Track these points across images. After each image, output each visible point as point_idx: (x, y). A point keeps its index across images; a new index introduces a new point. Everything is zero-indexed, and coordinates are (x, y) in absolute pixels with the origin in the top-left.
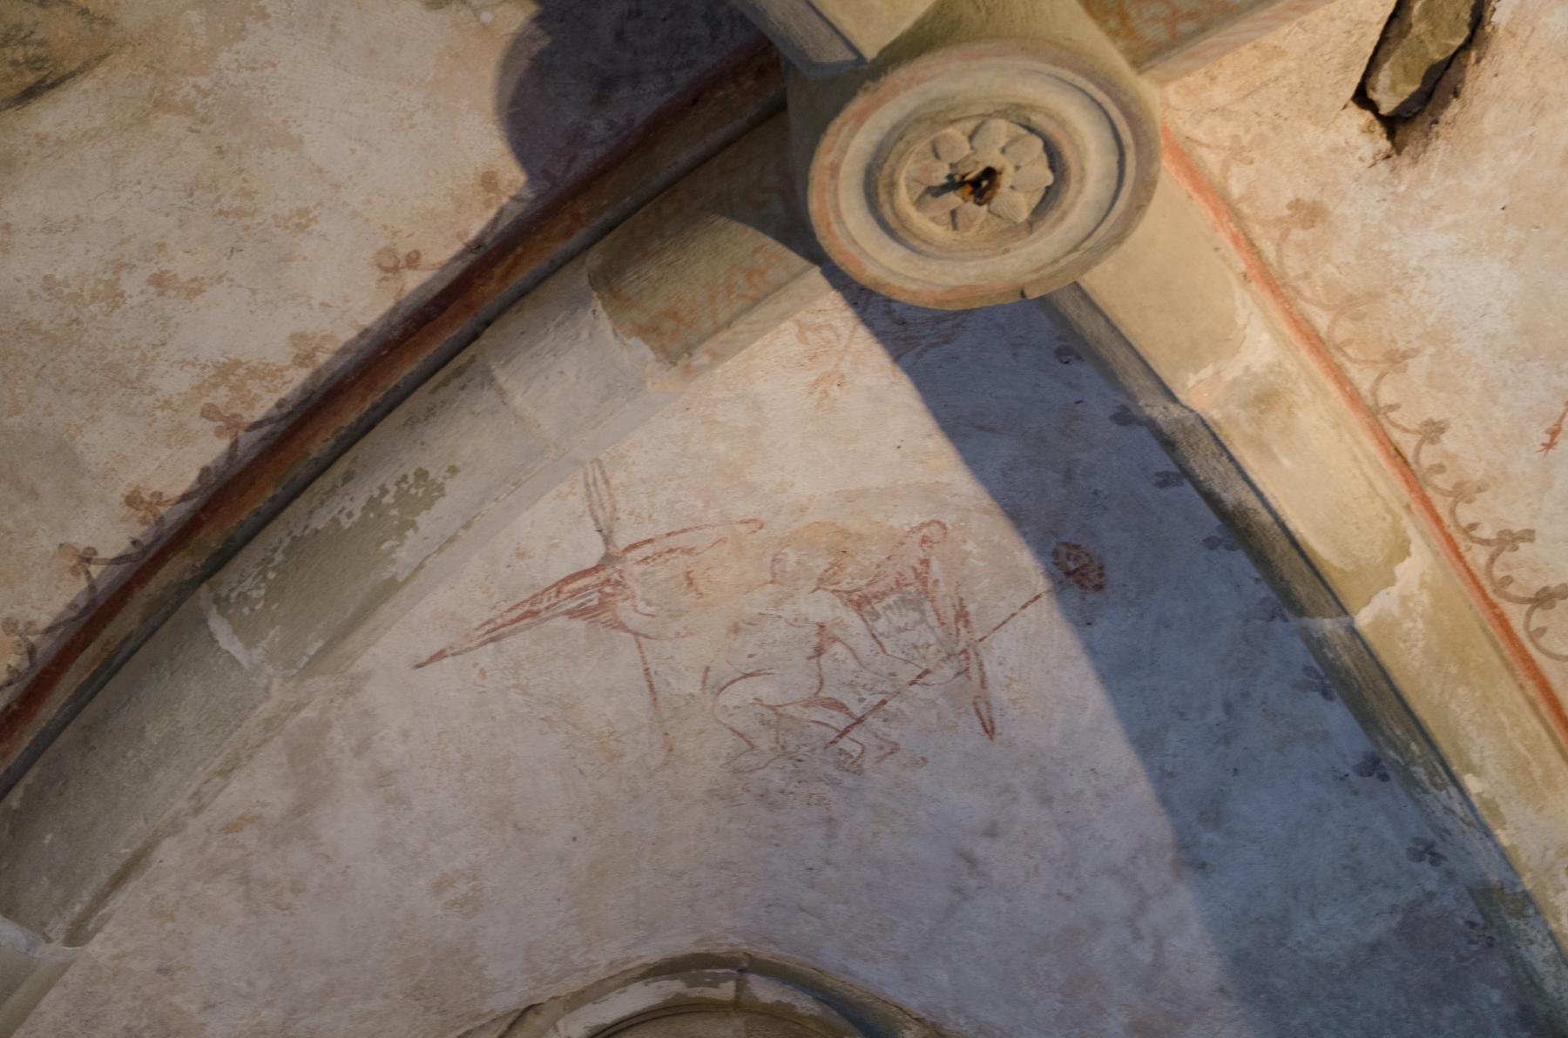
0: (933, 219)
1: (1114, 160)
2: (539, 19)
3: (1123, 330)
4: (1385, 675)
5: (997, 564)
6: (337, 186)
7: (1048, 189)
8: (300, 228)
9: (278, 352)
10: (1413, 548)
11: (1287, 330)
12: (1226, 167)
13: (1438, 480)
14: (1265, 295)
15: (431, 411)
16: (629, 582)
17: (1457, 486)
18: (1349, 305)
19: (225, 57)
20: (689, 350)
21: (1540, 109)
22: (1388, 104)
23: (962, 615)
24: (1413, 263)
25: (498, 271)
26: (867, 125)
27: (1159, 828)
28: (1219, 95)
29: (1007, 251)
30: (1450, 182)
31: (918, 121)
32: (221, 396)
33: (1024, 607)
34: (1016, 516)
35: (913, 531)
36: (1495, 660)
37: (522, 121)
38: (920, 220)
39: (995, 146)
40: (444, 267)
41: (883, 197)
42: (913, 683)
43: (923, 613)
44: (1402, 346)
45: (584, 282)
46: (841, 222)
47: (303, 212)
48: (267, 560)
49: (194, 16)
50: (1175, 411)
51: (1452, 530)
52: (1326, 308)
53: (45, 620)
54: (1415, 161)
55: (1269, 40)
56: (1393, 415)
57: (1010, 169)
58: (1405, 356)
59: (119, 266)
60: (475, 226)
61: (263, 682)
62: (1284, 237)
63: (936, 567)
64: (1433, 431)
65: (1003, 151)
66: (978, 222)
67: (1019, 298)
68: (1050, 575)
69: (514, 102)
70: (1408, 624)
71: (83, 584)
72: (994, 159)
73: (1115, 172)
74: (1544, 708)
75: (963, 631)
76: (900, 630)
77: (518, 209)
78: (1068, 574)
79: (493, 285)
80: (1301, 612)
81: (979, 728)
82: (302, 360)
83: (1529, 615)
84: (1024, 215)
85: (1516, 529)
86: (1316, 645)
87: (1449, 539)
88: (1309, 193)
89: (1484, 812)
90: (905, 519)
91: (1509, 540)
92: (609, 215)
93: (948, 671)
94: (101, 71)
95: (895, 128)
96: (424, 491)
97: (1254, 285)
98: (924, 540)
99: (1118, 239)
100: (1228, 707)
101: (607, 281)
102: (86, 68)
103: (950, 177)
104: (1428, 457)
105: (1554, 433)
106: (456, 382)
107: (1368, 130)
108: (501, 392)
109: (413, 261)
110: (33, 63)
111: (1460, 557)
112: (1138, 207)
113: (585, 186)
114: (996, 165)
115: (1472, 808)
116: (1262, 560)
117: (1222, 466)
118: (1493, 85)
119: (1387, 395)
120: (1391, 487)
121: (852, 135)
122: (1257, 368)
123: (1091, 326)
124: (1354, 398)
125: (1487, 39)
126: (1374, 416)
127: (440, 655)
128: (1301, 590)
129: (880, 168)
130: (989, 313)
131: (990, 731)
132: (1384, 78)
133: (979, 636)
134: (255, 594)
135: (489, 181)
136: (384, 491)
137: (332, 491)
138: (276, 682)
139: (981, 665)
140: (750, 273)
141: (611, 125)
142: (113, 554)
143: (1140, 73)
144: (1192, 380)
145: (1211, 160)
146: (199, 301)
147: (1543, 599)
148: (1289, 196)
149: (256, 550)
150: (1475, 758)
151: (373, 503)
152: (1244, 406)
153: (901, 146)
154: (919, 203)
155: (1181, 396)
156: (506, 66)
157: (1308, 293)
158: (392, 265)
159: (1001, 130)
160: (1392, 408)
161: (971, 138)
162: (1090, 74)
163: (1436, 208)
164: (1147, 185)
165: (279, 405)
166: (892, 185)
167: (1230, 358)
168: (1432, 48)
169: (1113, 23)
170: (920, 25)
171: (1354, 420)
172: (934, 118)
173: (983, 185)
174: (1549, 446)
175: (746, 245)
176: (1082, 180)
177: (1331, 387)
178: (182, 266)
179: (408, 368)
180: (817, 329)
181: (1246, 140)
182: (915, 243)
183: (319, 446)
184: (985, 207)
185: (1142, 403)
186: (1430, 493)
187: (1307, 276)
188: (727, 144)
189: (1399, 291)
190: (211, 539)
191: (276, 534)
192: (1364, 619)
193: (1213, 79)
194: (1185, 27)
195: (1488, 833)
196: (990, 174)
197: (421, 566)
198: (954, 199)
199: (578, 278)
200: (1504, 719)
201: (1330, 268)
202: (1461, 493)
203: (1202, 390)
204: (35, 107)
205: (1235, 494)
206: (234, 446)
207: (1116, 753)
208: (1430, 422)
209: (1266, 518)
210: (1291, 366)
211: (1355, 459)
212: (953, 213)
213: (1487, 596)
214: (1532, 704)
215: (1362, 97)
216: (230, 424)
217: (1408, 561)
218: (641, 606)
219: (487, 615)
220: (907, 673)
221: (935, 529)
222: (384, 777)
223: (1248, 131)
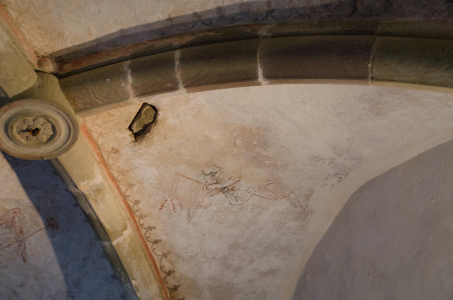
0: (22, 138)
1: (68, 132)
3: (67, 170)
4: (117, 256)
5: (32, 219)
7: (52, 136)
10: (128, 228)
11: (107, 175)
12: (98, 137)
13: (137, 213)
14: (103, 167)
17: (141, 215)
18: (122, 172)
21: (165, 138)
22: (135, 131)
23: (22, 232)
24: (137, 165)
26: (7, 113)
27: (64, 287)
28: (99, 122)
29: (39, 148)
30: (146, 150)
33: (38, 231)
34: (39, 209)
35: (12, 210)
36: (143, 255)
38: (18, 137)
41: (9, 130)
42: (6, 247)
43: (11, 230)
44: (132, 183)
50: (77, 191)
51: (138, 224)
52: (117, 172)
54: (139, 144)
55: (111, 112)
56: (129, 198)
57: (43, 129)
58: (133, 185)
62: (110, 155)
63: (16, 219)
64: (137, 202)
65: (41, 125)
66: (33, 140)
67: (41, 159)
68: (45, 224)
70: (124, 245)
72: (39, 126)
73: (68, 134)
74: (152, 266)
75: (21, 235)
76: (5, 234)
78: (50, 224)
80: (101, 240)
81: (22, 259)
83: (153, 245)
84: (45, 140)
85: (152, 226)
86: (104, 247)
87: (138, 227)
88: (116, 146)
89: (135, 289)
90: (10, 206)
91: (150, 228)
93: (16, 245)
95: (14, 115)
97: (101, 165)
98: (14, 212)
99: (67, 149)
100: (84, 260)
103: (27, 128)
104: (135, 208)
105: (162, 206)
107: (130, 135)
111: (139, 231)
112: (73, 143)
115: (133, 288)
116: (94, 227)
117: (87, 205)
118: (157, 132)
119: (128, 193)
120: (125, 213)
121: (3, 114)
122: (98, 183)
123: (59, 168)
124: (121, 193)
125: (156, 122)
126: (125, 198)
128: (102, 235)
129: (9, 123)
131: (25, 260)
132: (135, 125)
133: (25, 237)
139: (25, 244)
143: (77, 114)
144: (82, 184)
145: (95, 136)
147: (156, 242)
148: (111, 146)
150: (135, 277)
152: (94, 191)
153: (15, 119)
155: (79, 187)
157: (113, 168)
159: (41, 120)
160: (129, 196)
161: (34, 120)
162: (65, 112)
163: (143, 155)
164: (75, 139)
166: (12, 128)
167: (91, 180)
168: (145, 121)
169: (72, 102)
170: (24, 92)
171: (120, 198)
172: (25, 114)
173: (35, 132)
174: (161, 209)
176: (60, 135)
177: (116, 190)
181: (103, 132)
182: (17, 142)
184: (35, 137)
185: (70, 187)
186: (135, 216)
187: (113, 164)
189: (133, 171)
192: (114, 243)
193: (98, 118)
194: (88, 106)
195: (135, 294)
198: (28, 134)
200: (142, 268)
201: (119, 164)
202: (141, 217)
203: (84, 187)
205: (89, 211)
207: (56, 269)
208: (136, 201)
209: (95, 217)
210: (106, 184)
211: (118, 207)
212: (27, 137)
213: (144, 240)
214: (150, 265)
215: (130, 128)
217: (126, 231)
220: (5, 244)
221: (17, 210)
223: (104, 130)
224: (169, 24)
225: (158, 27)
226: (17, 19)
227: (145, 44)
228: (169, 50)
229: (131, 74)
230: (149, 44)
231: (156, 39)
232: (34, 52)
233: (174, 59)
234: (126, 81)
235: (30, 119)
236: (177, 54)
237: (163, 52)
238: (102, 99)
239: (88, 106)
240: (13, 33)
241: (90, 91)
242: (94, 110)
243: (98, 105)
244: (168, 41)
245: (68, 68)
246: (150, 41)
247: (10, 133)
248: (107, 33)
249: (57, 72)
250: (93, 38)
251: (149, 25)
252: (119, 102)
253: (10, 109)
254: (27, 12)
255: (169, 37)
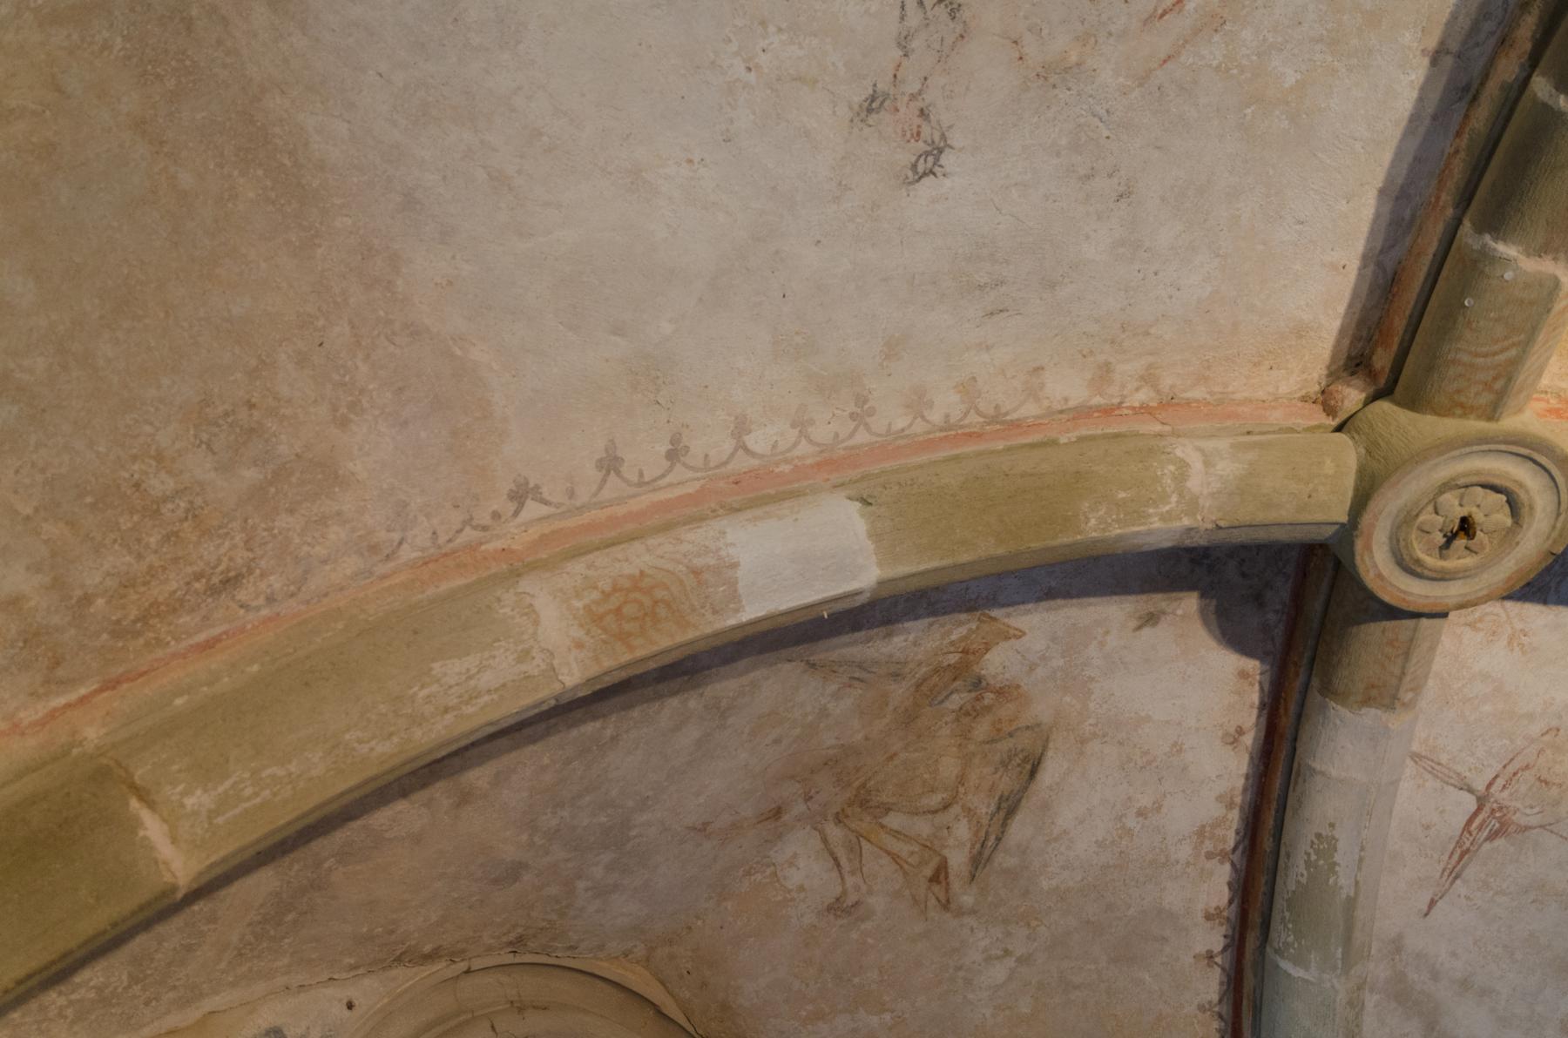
2: (1202, 596)
6: (1179, 724)
7: (1508, 502)
8: (1180, 751)
9: (1217, 811)
15: (1300, 801)
16: (1507, 803)
19: (1092, 705)
20: (1395, 697)
25: (1282, 711)
26: (1375, 548)
31: (1399, 527)
32: (1208, 845)
37: (1234, 639)
38: (1449, 564)
39: (1454, 507)
40: (1257, 725)
41: (1419, 570)
45: (1319, 698)
46: (1411, 594)
47: (1175, 744)
48: (1283, 918)
49: (1068, 699)
53: (1215, 997)
57: (1474, 509)
59: (1120, 818)
60: (1255, 697)
61: (1328, 985)
69: (1224, 634)
71: (1218, 970)
77: (1267, 678)
79: (1284, 719)
82: (1230, 806)
84: (1509, 522)
92: (1308, 654)
94: (1051, 745)
95: (1390, 538)
96: (1326, 845)
101: (1327, 690)
102: (1045, 748)
106: (1300, 780)
108: (1323, 773)
109: (1240, 731)
110: (1025, 760)
113: (1288, 645)
114: (1464, 512)
127: (1432, 903)
130: (1548, 569)
134: (1291, 939)
135: (1243, 675)
136: (1308, 854)
137: (1287, 868)
138: (1335, 981)
140: (1391, 643)
141: (1276, 612)
142: (1220, 948)
146: (1164, 810)
149: (1276, 917)
151: (1308, 864)
153: (1402, 543)
154: (1442, 557)
156: (1206, 623)
158: (1233, 739)
159: (1449, 499)
162: (1468, 444)
165: (1237, 833)
166: (1418, 561)
169: (1459, 411)
170: (1356, 490)
172: (1407, 519)
173: (1466, 527)
175: (1375, 632)
178: (1145, 801)
179: (1278, 783)
180: (1481, 620)
183: (1267, 843)
188: (1332, 587)
190: (1255, 917)
191: (1279, 903)
194: (1498, 385)
196: (1464, 520)
197: (1357, 883)
199: (1315, 697)
204: (1039, 776)
206: (1233, 864)
216: (1223, 855)
218: (1528, 811)
219: (1440, 868)
222: (1465, 984)
224: (1448, 61)
225: (1435, 97)
226: (1211, 393)
227: (1457, 152)
228: (1517, 100)
229: (1496, 240)
230: (1464, 142)
231: (1466, 116)
232: (1300, 404)
233: (1545, 105)
234: (1507, 262)
235: (1427, 516)
236: (1541, 86)
237: (1508, 119)
238: (1506, 343)
239: (1498, 385)
240: (1229, 423)
241: (1465, 358)
242: (1521, 378)
243: (1516, 363)
244: (1492, 89)
245: (1382, 360)
246: (1458, 134)
247: (1426, 572)
248: (1365, 228)
249: (1371, 390)
250: (1354, 265)
251: (1414, 118)
252: (1549, 311)
253: (1370, 537)
254: (1209, 368)
255: (1485, 77)
